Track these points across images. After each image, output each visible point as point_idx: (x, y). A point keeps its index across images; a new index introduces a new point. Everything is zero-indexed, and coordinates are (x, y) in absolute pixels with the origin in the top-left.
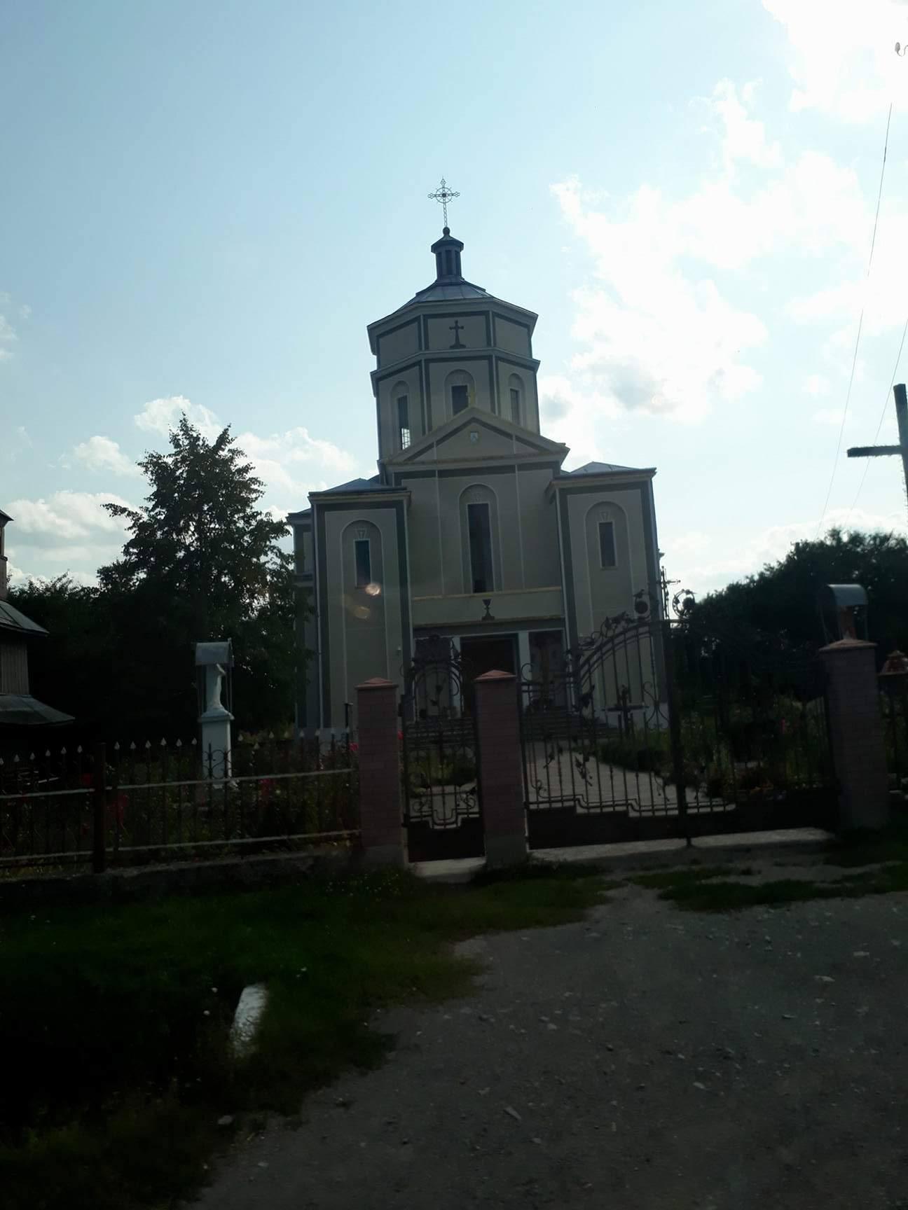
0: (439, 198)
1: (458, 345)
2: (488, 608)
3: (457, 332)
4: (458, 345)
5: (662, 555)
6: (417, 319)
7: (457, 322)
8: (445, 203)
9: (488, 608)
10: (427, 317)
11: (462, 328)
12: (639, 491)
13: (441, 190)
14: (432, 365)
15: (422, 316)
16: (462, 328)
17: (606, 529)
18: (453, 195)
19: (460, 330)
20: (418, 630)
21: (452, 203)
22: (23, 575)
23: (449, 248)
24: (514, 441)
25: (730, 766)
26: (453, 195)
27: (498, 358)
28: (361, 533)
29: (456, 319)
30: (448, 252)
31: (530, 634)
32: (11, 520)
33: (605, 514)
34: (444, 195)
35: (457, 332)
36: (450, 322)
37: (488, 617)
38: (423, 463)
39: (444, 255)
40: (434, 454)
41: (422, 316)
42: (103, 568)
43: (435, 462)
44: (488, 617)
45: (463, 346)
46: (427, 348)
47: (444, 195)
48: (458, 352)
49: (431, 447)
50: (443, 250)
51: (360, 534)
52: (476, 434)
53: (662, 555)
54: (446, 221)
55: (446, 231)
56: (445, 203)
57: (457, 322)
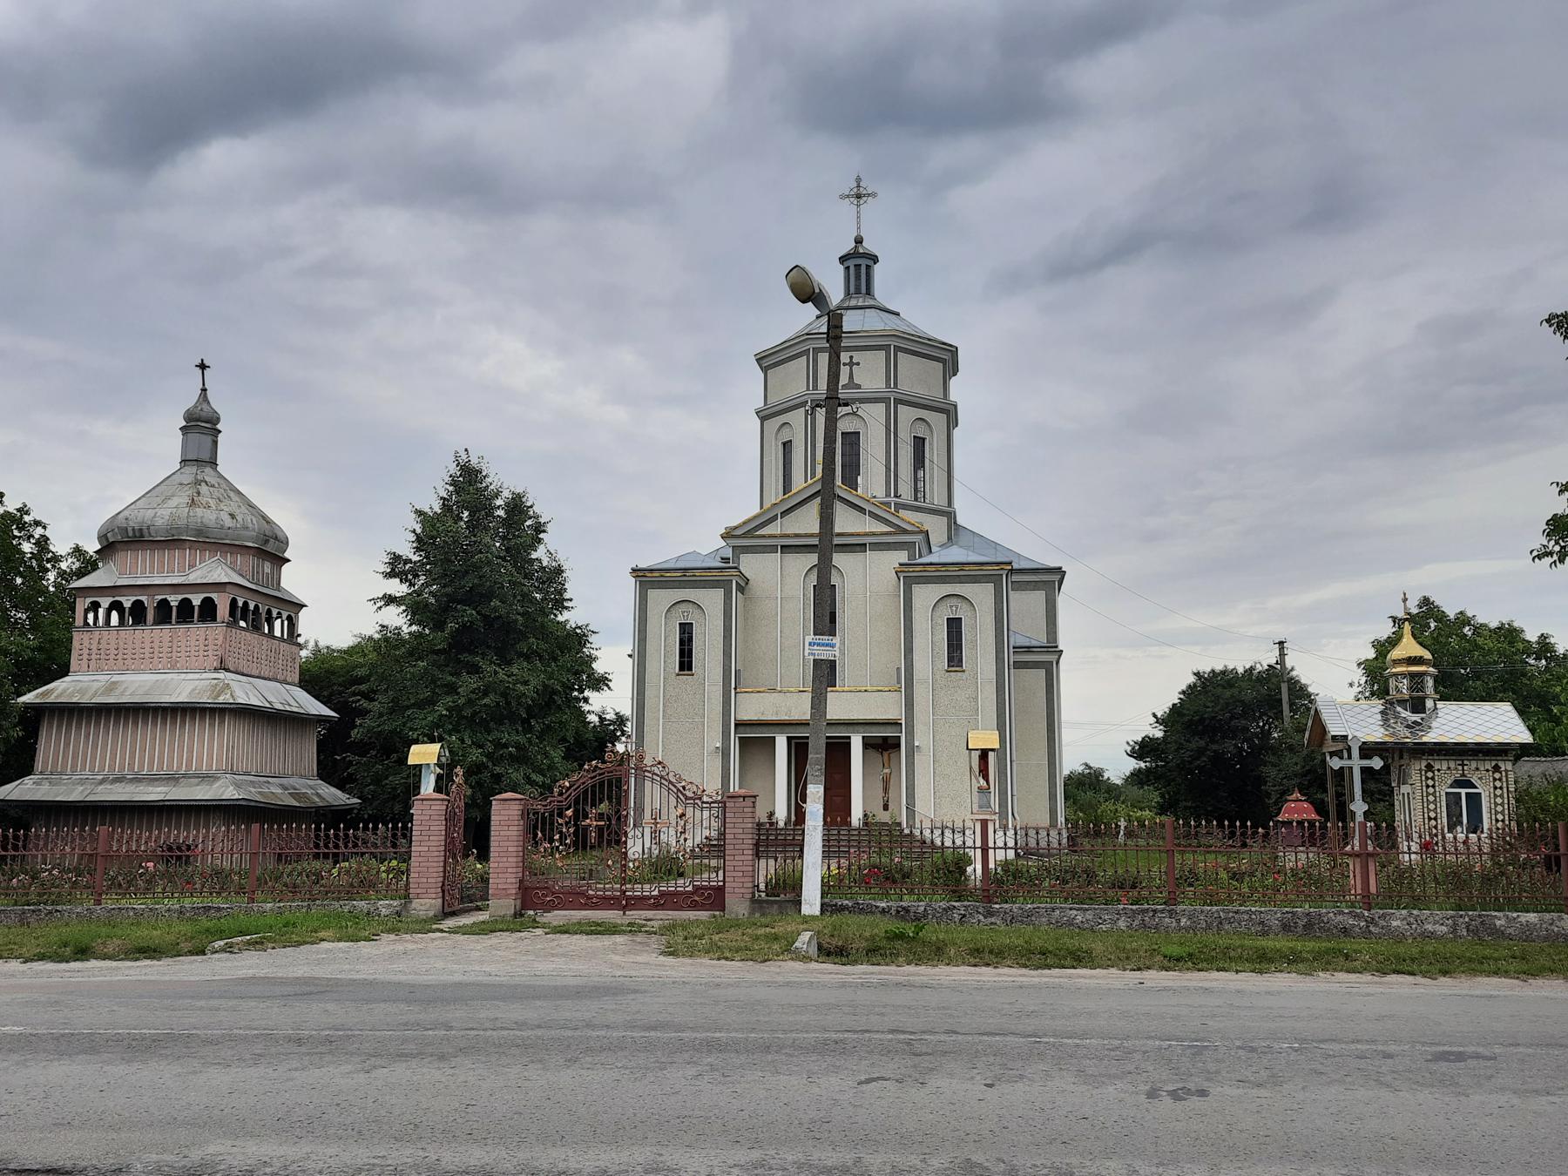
0: (852, 199)
3: (851, 369)
5: (1197, 674)
6: (806, 352)
7: (851, 357)
8: (858, 206)
10: (897, 349)
11: (858, 364)
15: (811, 350)
16: (858, 364)
17: (954, 625)
18: (848, 196)
20: (739, 725)
21: (868, 206)
22: (1066, 772)
23: (858, 261)
26: (848, 196)
27: (898, 401)
28: (686, 614)
29: (850, 354)
30: (858, 266)
31: (863, 737)
32: (306, 606)
33: (954, 608)
34: (859, 196)
35: (851, 369)
38: (763, 536)
39: (852, 269)
41: (811, 350)
42: (1223, 672)
45: (859, 387)
47: (859, 196)
49: (774, 518)
50: (851, 263)
53: (1197, 674)
54: (858, 228)
55: (859, 241)
56: (858, 206)
57: (851, 357)
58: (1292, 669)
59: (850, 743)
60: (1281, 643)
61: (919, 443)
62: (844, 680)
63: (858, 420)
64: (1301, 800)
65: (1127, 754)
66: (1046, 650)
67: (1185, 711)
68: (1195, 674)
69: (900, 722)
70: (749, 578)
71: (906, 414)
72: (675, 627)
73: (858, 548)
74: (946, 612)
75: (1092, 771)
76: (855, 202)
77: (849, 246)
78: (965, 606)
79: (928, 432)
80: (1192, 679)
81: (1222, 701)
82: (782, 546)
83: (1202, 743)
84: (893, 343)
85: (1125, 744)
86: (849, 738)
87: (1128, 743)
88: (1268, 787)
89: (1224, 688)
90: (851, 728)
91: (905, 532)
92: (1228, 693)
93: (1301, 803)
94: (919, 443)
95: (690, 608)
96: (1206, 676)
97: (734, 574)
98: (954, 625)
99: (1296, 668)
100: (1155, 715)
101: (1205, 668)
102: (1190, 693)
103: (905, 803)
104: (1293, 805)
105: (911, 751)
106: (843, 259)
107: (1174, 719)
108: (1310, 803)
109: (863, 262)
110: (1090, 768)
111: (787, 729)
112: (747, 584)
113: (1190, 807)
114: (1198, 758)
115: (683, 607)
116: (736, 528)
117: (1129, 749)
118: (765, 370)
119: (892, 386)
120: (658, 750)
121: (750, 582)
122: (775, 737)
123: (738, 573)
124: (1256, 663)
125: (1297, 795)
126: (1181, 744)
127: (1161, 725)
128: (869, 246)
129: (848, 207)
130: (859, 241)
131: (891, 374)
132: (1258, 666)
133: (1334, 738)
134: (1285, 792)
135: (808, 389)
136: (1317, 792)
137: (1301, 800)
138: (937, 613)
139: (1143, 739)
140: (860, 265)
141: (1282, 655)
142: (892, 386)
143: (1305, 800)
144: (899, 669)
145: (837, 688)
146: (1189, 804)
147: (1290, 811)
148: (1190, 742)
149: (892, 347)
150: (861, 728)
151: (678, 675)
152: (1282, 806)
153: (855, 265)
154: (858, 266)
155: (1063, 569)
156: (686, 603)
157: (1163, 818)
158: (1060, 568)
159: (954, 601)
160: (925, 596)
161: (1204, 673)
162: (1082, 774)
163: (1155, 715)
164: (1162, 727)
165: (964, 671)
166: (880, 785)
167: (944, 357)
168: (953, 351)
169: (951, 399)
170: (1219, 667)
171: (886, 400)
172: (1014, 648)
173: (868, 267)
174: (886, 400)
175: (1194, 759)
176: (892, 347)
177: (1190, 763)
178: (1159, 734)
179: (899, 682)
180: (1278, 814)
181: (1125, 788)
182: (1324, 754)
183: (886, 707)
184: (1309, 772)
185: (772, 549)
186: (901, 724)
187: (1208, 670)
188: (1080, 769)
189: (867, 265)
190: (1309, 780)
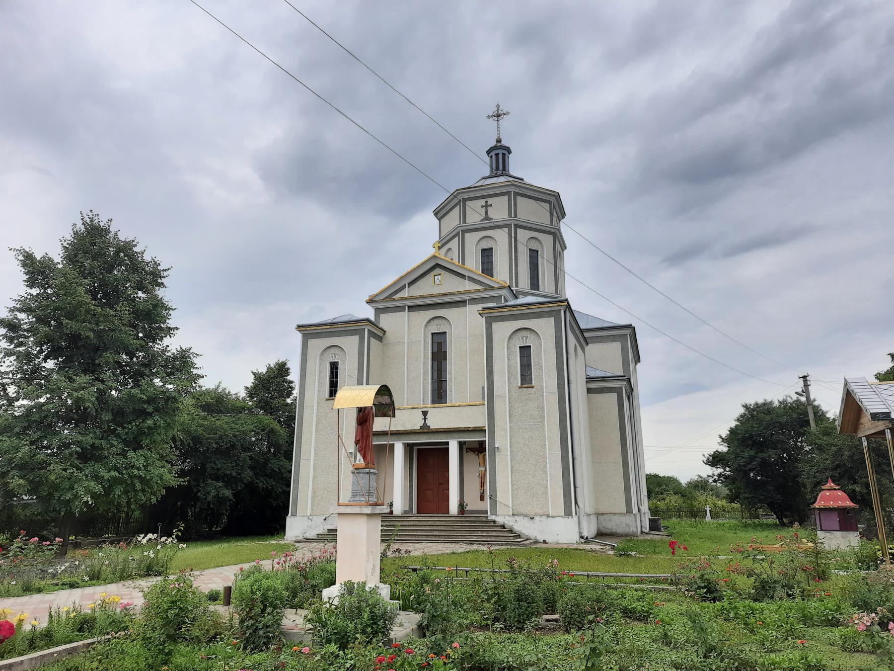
0: (494, 118)
1: (487, 218)
2: (425, 419)
4: (487, 218)
5: (746, 407)
7: (486, 202)
8: (498, 121)
9: (425, 419)
10: (516, 194)
11: (491, 205)
12: (552, 319)
13: (496, 112)
14: (467, 235)
16: (491, 205)
17: (525, 351)
18: (492, 116)
19: (489, 208)
21: (505, 121)
23: (497, 152)
24: (467, 281)
25: (104, 386)
26: (492, 116)
27: (516, 226)
29: (485, 200)
30: (497, 155)
36: (482, 202)
37: (425, 425)
39: (494, 157)
40: (405, 293)
42: (764, 404)
43: (406, 299)
44: (425, 425)
45: (492, 219)
46: (516, 216)
48: (488, 224)
49: (403, 287)
50: (493, 154)
51: (332, 357)
52: (439, 276)
55: (499, 141)
56: (498, 121)
57: (486, 202)
58: (814, 400)
59: (448, 449)
60: (804, 377)
61: (534, 255)
62: (452, 400)
63: (493, 240)
64: (835, 489)
65: (704, 462)
66: (616, 378)
67: (738, 431)
68: (743, 406)
69: (484, 429)
70: (385, 330)
71: (523, 235)
72: (326, 366)
73: (461, 304)
74: (519, 342)
75: (702, 479)
76: (496, 119)
77: (494, 143)
78: (531, 336)
79: (540, 247)
80: (742, 411)
81: (764, 423)
82: (409, 307)
83: (753, 453)
84: (513, 189)
85: (702, 456)
86: (447, 443)
87: (704, 456)
88: (803, 478)
89: (765, 414)
90: (449, 435)
91: (492, 288)
92: (768, 418)
93: (834, 492)
94: (534, 255)
95: (336, 350)
96: (752, 407)
97: (365, 324)
98: (525, 351)
99: (817, 399)
100: (721, 437)
101: (751, 401)
102: (742, 419)
103: (488, 494)
104: (828, 494)
105: (494, 450)
106: (488, 152)
107: (734, 437)
108: (844, 492)
109: (500, 152)
110: (701, 477)
111: (403, 437)
112: (384, 334)
113: (747, 498)
114: (750, 463)
115: (333, 350)
116: (376, 295)
117: (705, 459)
118: (440, 219)
119: (513, 216)
120: (310, 456)
121: (387, 333)
122: (394, 444)
123: (368, 323)
124: (787, 396)
125: (830, 484)
126: (737, 454)
127: (725, 442)
128: (504, 143)
129: (493, 123)
130: (499, 141)
131: (513, 210)
132: (789, 398)
133: (875, 416)
134: (817, 485)
135: (460, 222)
136: (848, 484)
137: (835, 489)
138: (512, 342)
139: (715, 452)
140: (499, 154)
141: (806, 385)
142: (513, 216)
143: (838, 489)
144: (483, 388)
145: (448, 404)
146: (747, 495)
147: (825, 498)
148: (744, 452)
149: (512, 193)
150: (456, 435)
151: (327, 400)
152: (817, 495)
153: (495, 154)
154: (497, 155)
155: (633, 326)
156: (335, 348)
157: (733, 505)
158: (631, 325)
159: (524, 333)
160: (503, 330)
161: (750, 405)
162: (697, 481)
163: (721, 437)
164: (726, 444)
165: (533, 387)
166: (478, 481)
167: (551, 200)
168: (557, 196)
169: (512, 173)
170: (761, 401)
171: (508, 226)
172: (589, 379)
173: (504, 154)
174: (508, 226)
175: (747, 464)
176: (512, 193)
177: (745, 466)
178: (724, 449)
179: (484, 399)
180: (814, 503)
181: (721, 488)
182: (861, 438)
183: (476, 418)
184: (838, 466)
185: (401, 309)
186: (485, 430)
187: (753, 403)
188: (696, 478)
189: (503, 153)
190: (839, 473)
